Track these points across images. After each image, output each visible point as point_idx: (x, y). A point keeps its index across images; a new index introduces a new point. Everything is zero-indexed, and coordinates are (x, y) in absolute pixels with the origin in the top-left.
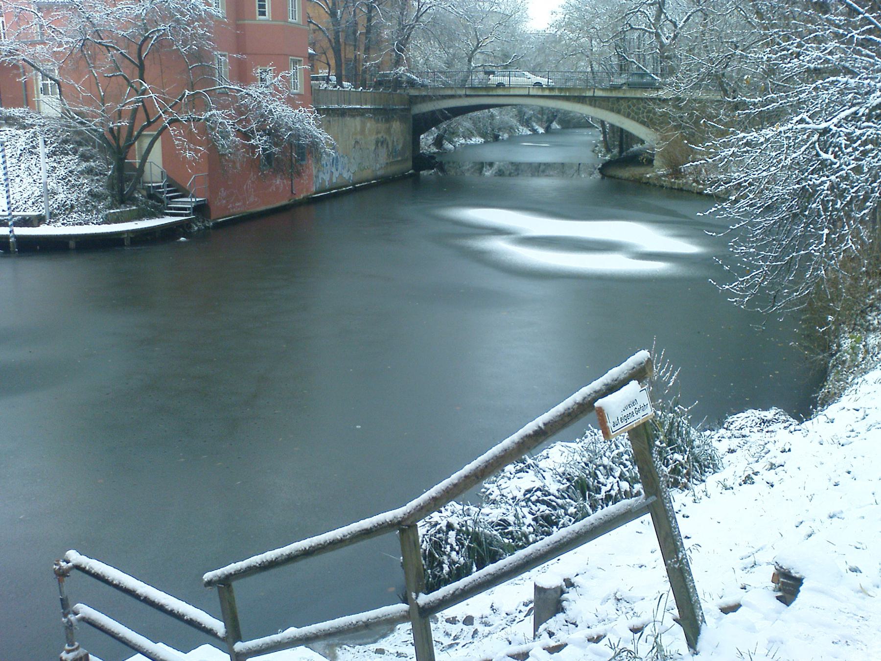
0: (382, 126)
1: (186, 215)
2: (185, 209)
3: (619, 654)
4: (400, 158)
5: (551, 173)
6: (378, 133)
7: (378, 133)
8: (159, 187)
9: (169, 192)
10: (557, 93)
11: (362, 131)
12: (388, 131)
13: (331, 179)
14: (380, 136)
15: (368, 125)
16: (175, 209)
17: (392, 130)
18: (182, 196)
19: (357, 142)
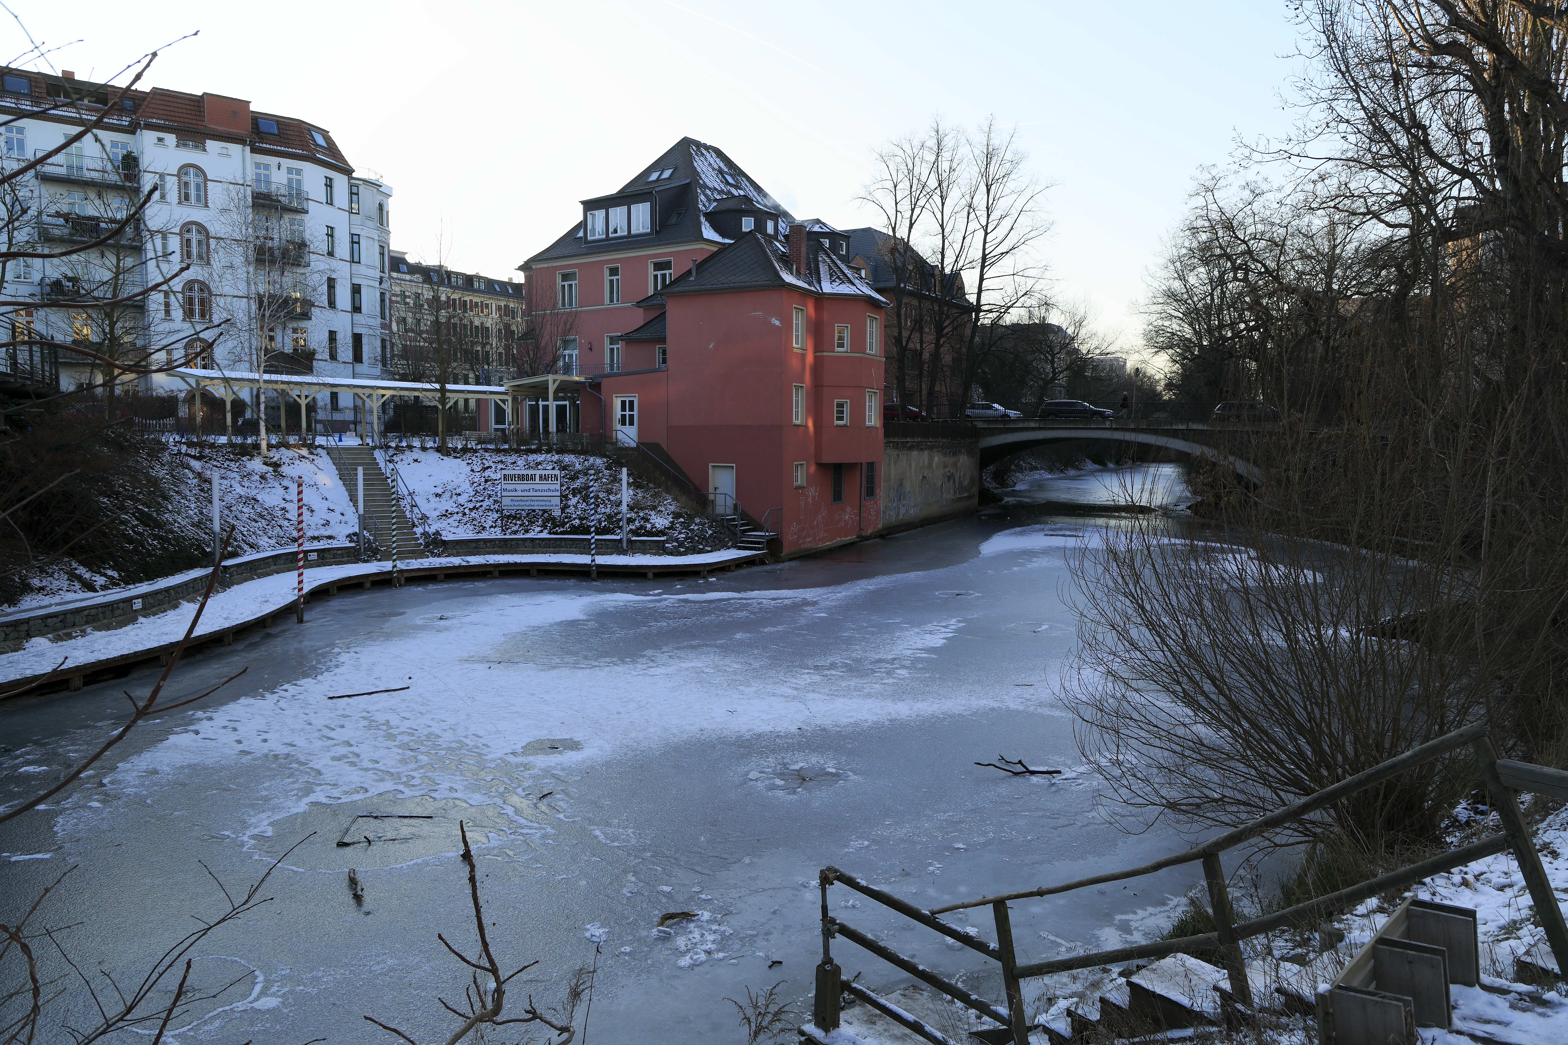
0: (950, 460)
1: (759, 549)
2: (758, 543)
3: (1460, 90)
4: (966, 495)
5: (419, 621)
6: (945, 467)
7: (945, 467)
8: (734, 520)
9: (743, 525)
10: (202, 193)
11: (930, 466)
12: (955, 465)
13: (898, 514)
14: (947, 470)
15: (936, 458)
16: (748, 542)
17: (959, 464)
18: (754, 530)
19: (924, 477)
